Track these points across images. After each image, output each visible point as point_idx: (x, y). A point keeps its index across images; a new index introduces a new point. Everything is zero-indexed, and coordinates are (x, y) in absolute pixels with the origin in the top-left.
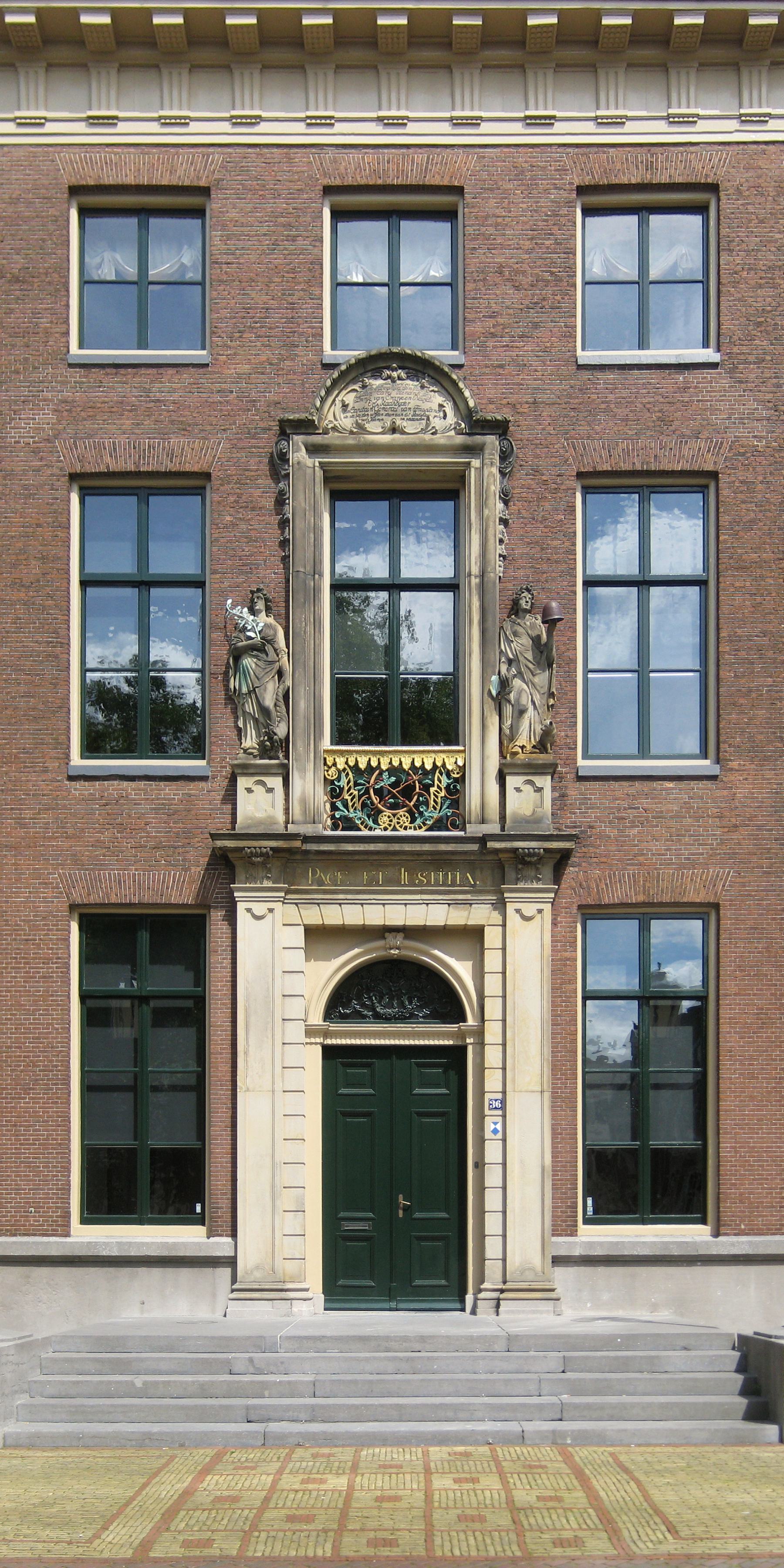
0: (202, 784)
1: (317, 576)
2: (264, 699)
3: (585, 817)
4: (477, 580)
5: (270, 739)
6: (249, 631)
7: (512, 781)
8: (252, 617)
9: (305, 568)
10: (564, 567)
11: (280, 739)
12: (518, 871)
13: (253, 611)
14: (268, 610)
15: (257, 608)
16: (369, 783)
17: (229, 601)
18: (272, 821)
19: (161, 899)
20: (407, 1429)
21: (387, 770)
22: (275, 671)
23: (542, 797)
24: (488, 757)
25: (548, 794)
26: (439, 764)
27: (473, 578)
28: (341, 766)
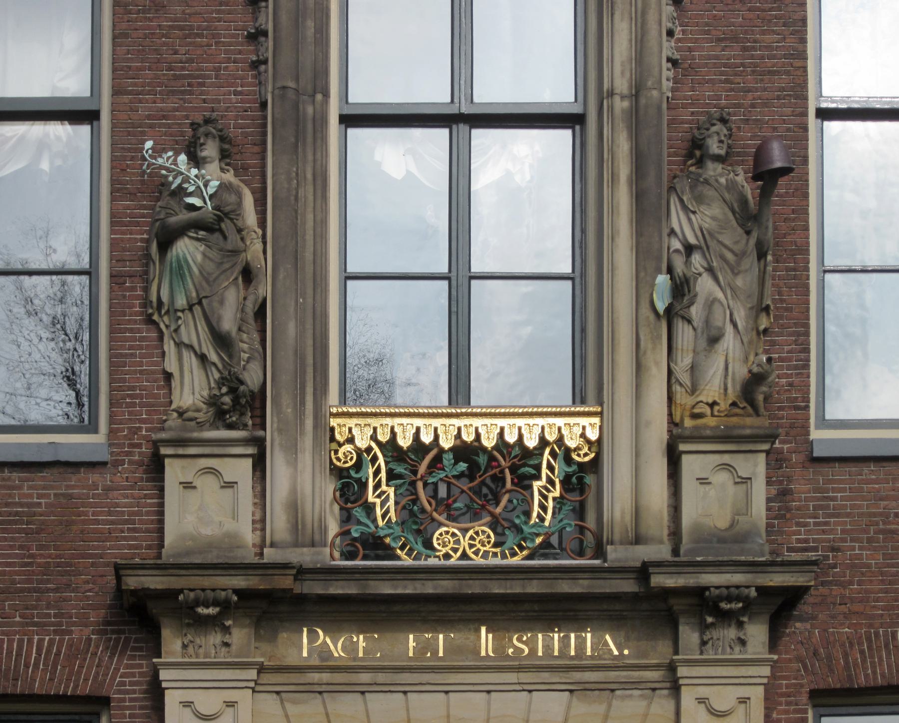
0: (93, 477)
1: (319, 97)
2: (220, 318)
3: (824, 532)
4: (626, 104)
5: (233, 391)
6: (191, 194)
7: (691, 466)
8: (194, 171)
9: (297, 79)
10: (783, 81)
11: (251, 391)
12: (704, 627)
13: (196, 160)
14: (224, 155)
15: (204, 154)
16: (415, 473)
17: (149, 144)
18: (232, 541)
19: (15, 686)
20: (593, 155)
21: (451, 449)
22: (239, 268)
23: (748, 496)
24: (648, 424)
25: (760, 492)
26: (551, 437)
27: (617, 99)
28: (362, 442)
